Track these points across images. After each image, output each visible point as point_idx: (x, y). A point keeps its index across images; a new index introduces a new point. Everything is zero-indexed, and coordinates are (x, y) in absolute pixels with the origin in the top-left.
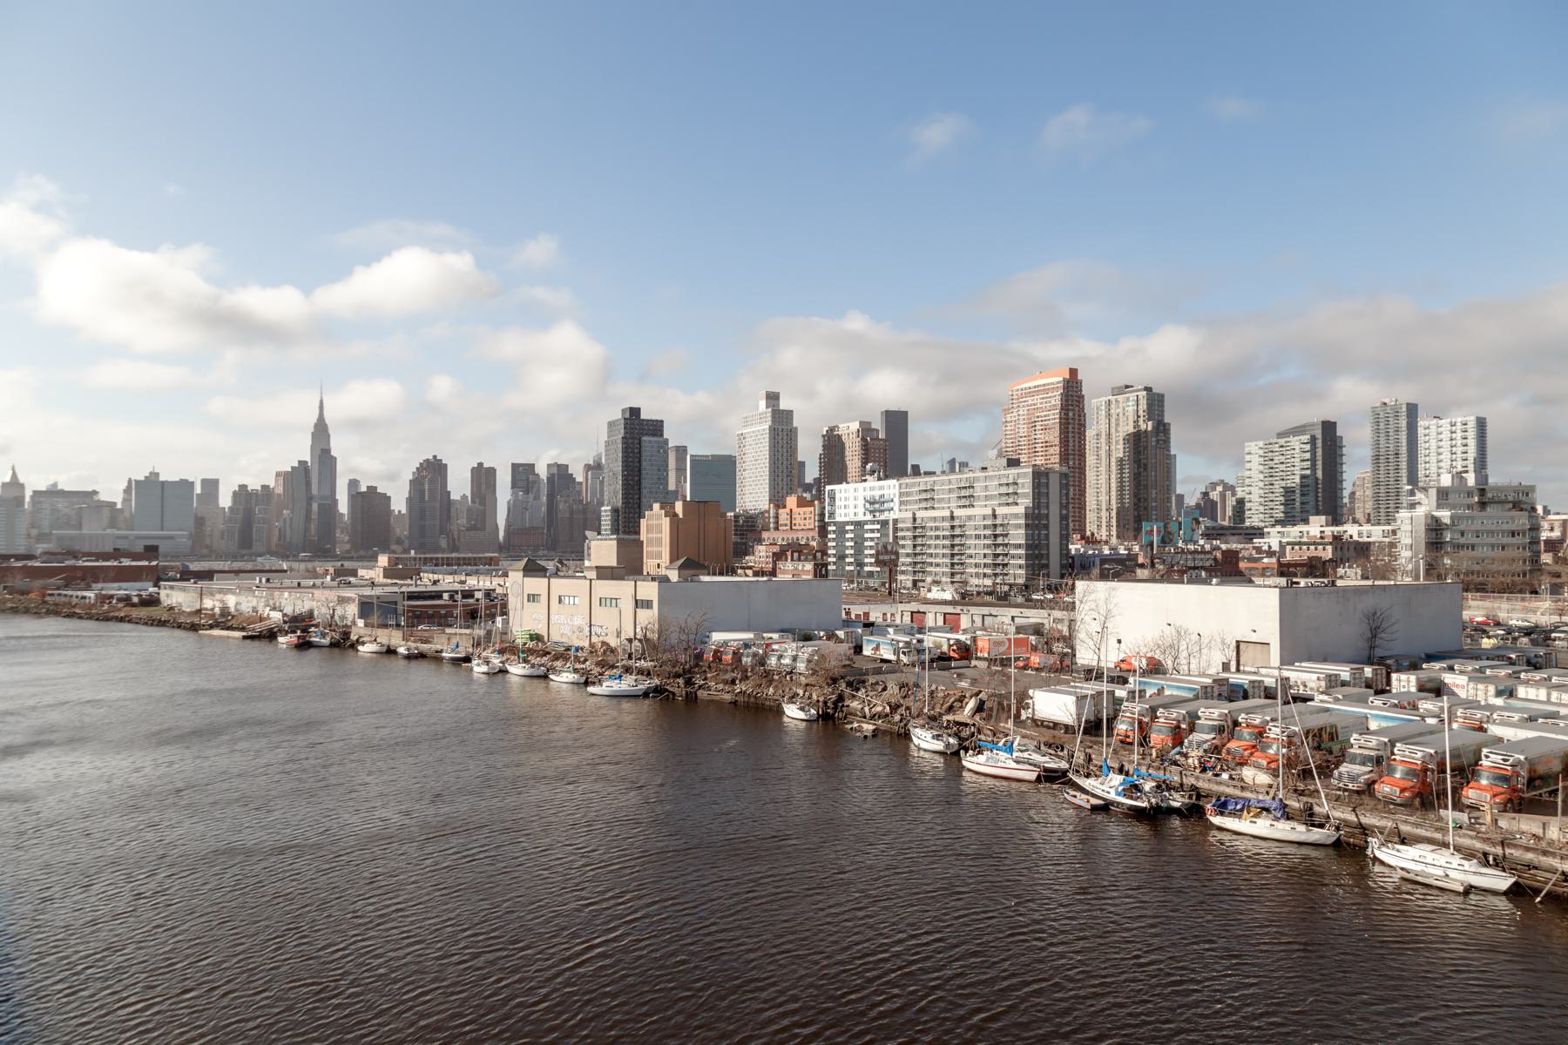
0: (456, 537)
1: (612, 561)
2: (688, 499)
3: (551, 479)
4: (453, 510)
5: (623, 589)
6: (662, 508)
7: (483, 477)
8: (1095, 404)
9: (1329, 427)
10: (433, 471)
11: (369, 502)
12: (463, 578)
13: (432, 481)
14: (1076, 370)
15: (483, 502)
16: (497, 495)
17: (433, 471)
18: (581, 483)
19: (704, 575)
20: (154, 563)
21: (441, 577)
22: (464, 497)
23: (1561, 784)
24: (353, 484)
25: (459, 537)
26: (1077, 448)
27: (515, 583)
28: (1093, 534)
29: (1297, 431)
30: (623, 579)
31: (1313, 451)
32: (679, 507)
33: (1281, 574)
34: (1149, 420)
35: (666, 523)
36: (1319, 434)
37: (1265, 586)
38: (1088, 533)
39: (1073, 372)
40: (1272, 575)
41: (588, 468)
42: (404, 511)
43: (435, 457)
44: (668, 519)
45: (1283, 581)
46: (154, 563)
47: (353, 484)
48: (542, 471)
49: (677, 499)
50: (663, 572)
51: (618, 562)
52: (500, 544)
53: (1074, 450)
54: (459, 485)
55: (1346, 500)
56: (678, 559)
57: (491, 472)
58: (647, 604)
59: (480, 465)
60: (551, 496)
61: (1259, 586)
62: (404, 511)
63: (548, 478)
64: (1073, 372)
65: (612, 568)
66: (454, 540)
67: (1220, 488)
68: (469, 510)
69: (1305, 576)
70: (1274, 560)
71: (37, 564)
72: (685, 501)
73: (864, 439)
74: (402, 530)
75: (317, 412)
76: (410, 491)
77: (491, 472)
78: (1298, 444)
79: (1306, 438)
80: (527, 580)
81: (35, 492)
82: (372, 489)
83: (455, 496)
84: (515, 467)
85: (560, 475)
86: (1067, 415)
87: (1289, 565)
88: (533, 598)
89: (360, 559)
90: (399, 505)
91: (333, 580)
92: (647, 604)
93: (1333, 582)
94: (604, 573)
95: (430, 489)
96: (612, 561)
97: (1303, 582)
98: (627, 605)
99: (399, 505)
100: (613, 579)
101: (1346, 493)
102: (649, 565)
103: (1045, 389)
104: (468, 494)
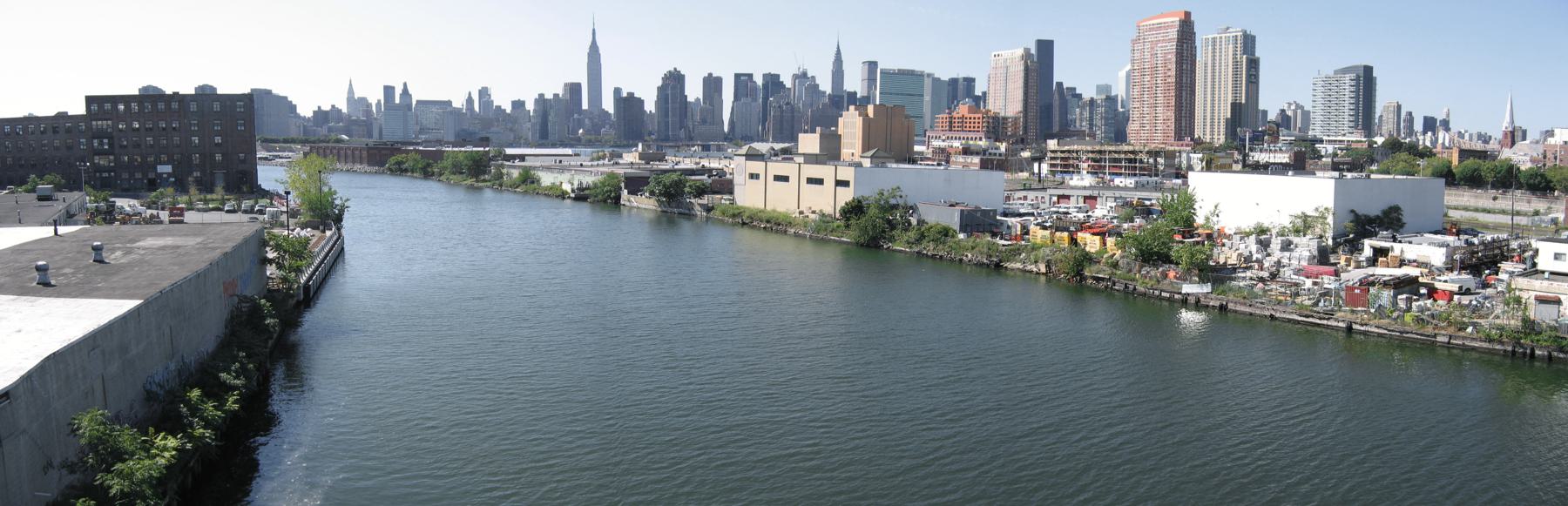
0: (691, 130)
1: (816, 150)
2: (878, 103)
3: (765, 86)
4: (689, 109)
5: (825, 171)
6: (856, 109)
7: (712, 85)
8: (1202, 35)
9: (1368, 70)
10: (674, 81)
11: (628, 104)
12: (698, 160)
13: (674, 88)
14: (1190, 13)
15: (711, 104)
16: (723, 97)
17: (674, 81)
18: (790, 89)
19: (890, 162)
20: (487, 149)
21: (681, 159)
22: (698, 100)
23: (1107, 164)
24: (617, 91)
25: (693, 128)
26: (1189, 82)
27: (736, 166)
28: (1200, 137)
29: (1345, 71)
30: (825, 164)
31: (1357, 85)
32: (870, 109)
33: (1334, 169)
34: (1244, 54)
35: (859, 121)
36: (1361, 73)
37: (1324, 178)
38: (1196, 136)
39: (1188, 14)
40: (1328, 170)
41: (795, 77)
42: (653, 111)
43: (675, 69)
44: (861, 118)
45: (1336, 174)
46: (487, 149)
47: (617, 91)
48: (759, 81)
49: (869, 103)
50: (857, 159)
51: (820, 151)
52: (725, 134)
53: (1186, 83)
54: (694, 91)
55: (1377, 121)
56: (869, 150)
57: (719, 81)
58: (845, 184)
59: (710, 75)
60: (766, 99)
61: (1320, 177)
62: (653, 111)
63: (763, 85)
64: (1188, 14)
65: (817, 155)
66: (690, 131)
67: (1293, 107)
68: (702, 110)
69: (1349, 170)
70: (1330, 160)
71: (421, 148)
72: (875, 105)
73: (1026, 63)
74: (653, 126)
75: (591, 39)
76: (658, 96)
77: (719, 81)
78: (1348, 79)
79: (1353, 76)
80: (749, 163)
81: (417, 101)
82: (631, 95)
83: (691, 99)
84: (737, 76)
85: (773, 81)
86: (1183, 46)
87: (1339, 163)
88: (754, 176)
89: (624, 146)
90: (650, 106)
91: (609, 161)
92: (845, 184)
93: (1369, 176)
94: (811, 159)
95: (672, 94)
96: (816, 150)
97: (1349, 175)
98: (829, 183)
99: (650, 106)
100: (817, 163)
101: (1377, 116)
102: (846, 152)
103: (1168, 26)
104: (701, 97)
